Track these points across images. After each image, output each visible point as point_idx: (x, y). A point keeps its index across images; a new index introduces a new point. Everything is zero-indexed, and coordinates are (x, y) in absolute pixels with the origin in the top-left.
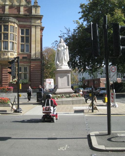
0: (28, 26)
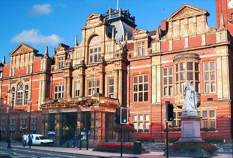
0: (212, 59)
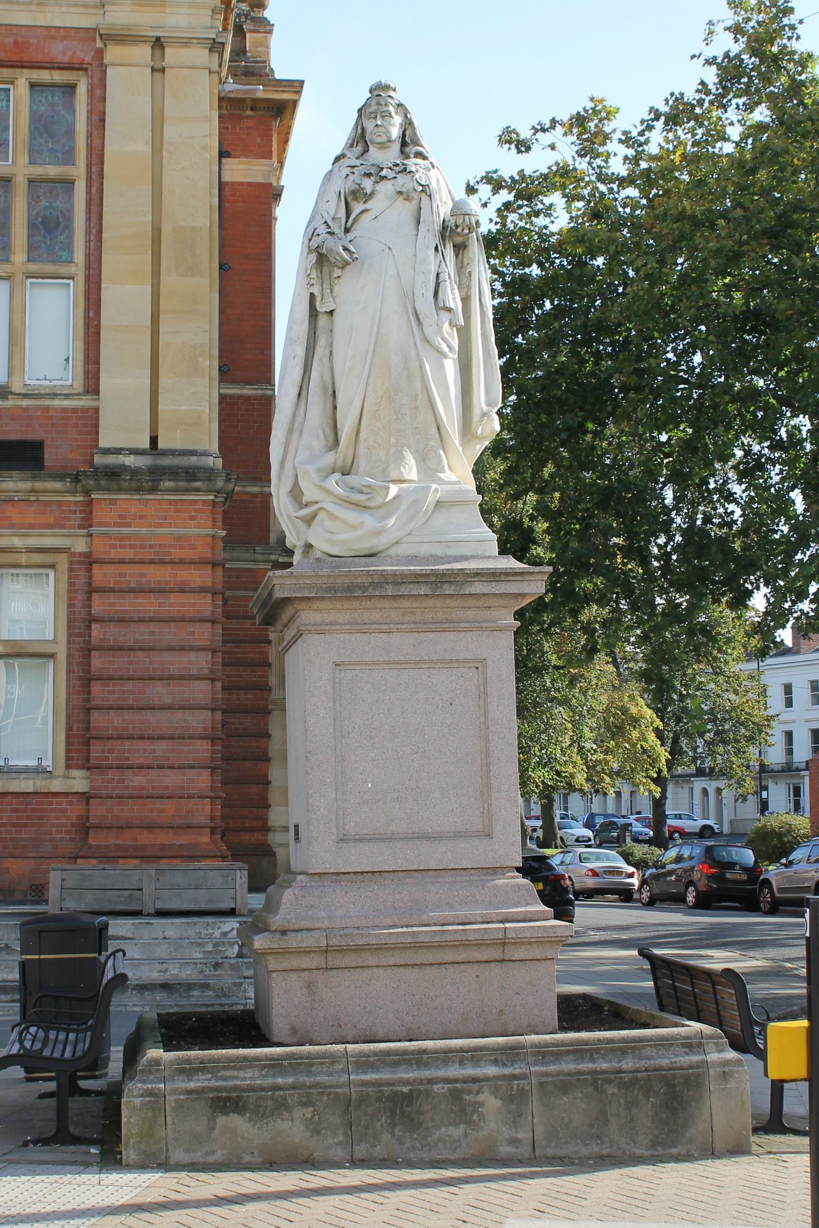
0: (58, 50)
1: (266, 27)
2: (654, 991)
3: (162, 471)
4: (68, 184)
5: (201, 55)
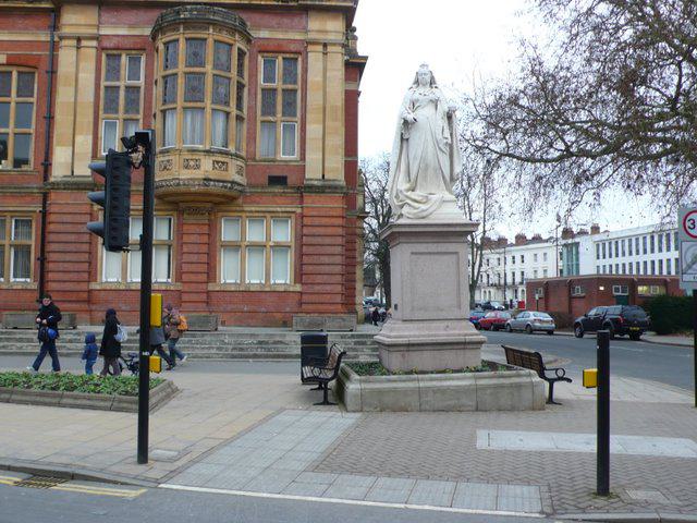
0: (293, 47)
1: (355, 38)
2: (612, 363)
3: (325, 188)
4: (295, 91)
5: (339, 49)
